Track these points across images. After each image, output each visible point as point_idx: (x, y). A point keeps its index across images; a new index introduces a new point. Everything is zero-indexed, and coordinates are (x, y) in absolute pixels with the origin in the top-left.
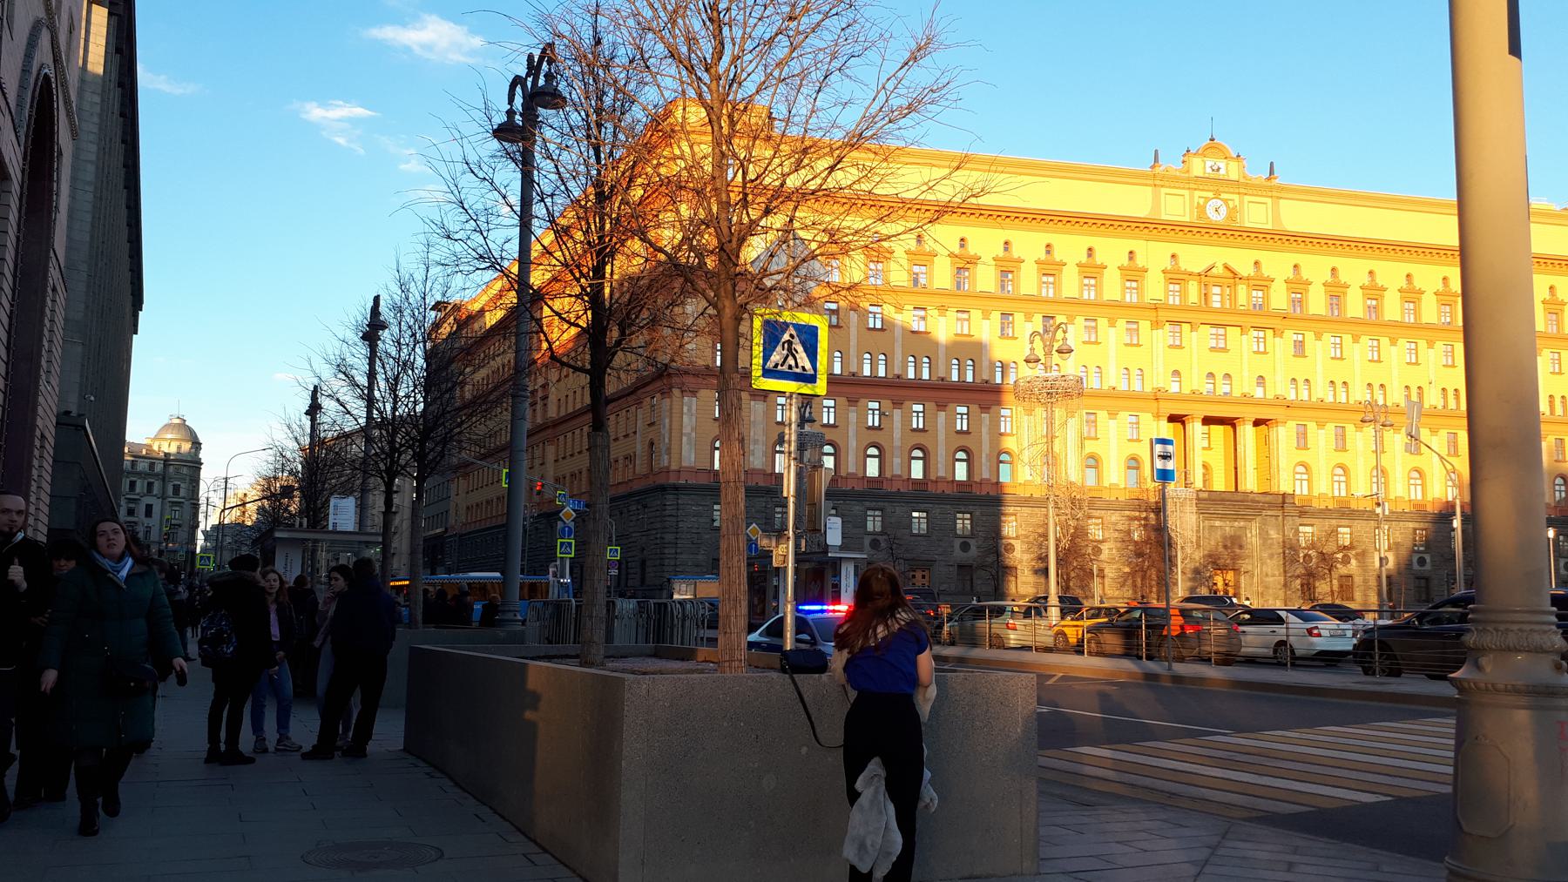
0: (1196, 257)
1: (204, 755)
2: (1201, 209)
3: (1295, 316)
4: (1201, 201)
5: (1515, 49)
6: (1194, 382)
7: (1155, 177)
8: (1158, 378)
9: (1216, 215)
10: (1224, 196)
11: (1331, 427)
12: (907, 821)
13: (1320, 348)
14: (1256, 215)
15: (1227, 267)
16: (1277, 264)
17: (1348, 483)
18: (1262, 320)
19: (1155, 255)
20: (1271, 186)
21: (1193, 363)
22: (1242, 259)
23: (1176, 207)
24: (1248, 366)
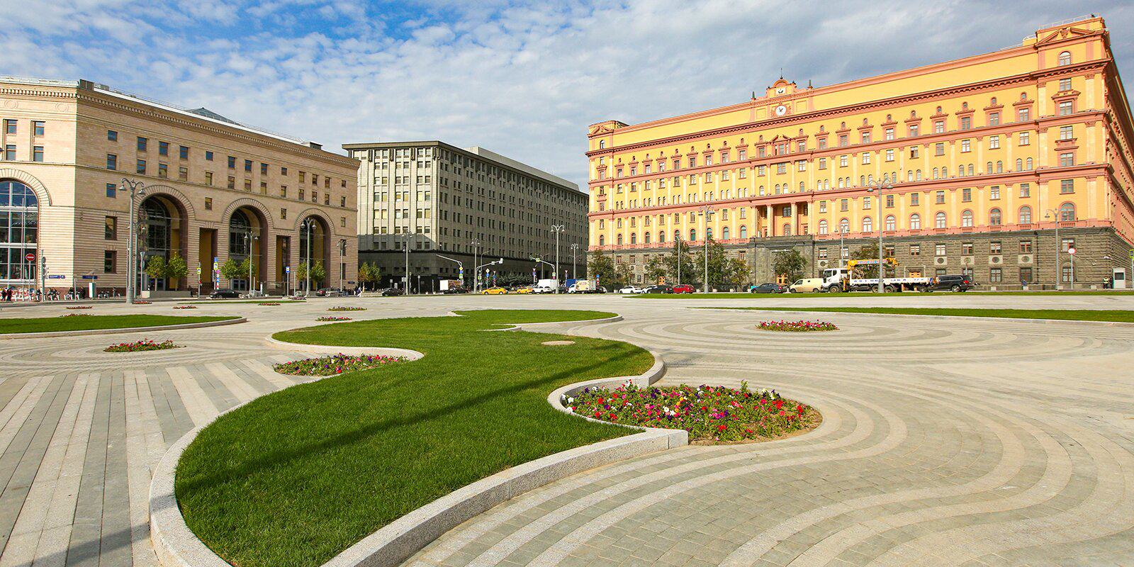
0: (769, 134)
1: (236, 161)
2: (774, 113)
3: (823, 152)
4: (774, 109)
5: (111, 350)
6: (769, 190)
7: (754, 103)
8: (752, 191)
9: (780, 113)
10: (784, 103)
11: (839, 201)
12: (546, 293)
13: (832, 164)
14: (801, 108)
15: (784, 137)
16: (811, 128)
17: (972, 222)
18: (803, 157)
19: (751, 138)
20: (812, 92)
21: (768, 183)
22: (791, 131)
23: (762, 115)
24: (792, 180)
